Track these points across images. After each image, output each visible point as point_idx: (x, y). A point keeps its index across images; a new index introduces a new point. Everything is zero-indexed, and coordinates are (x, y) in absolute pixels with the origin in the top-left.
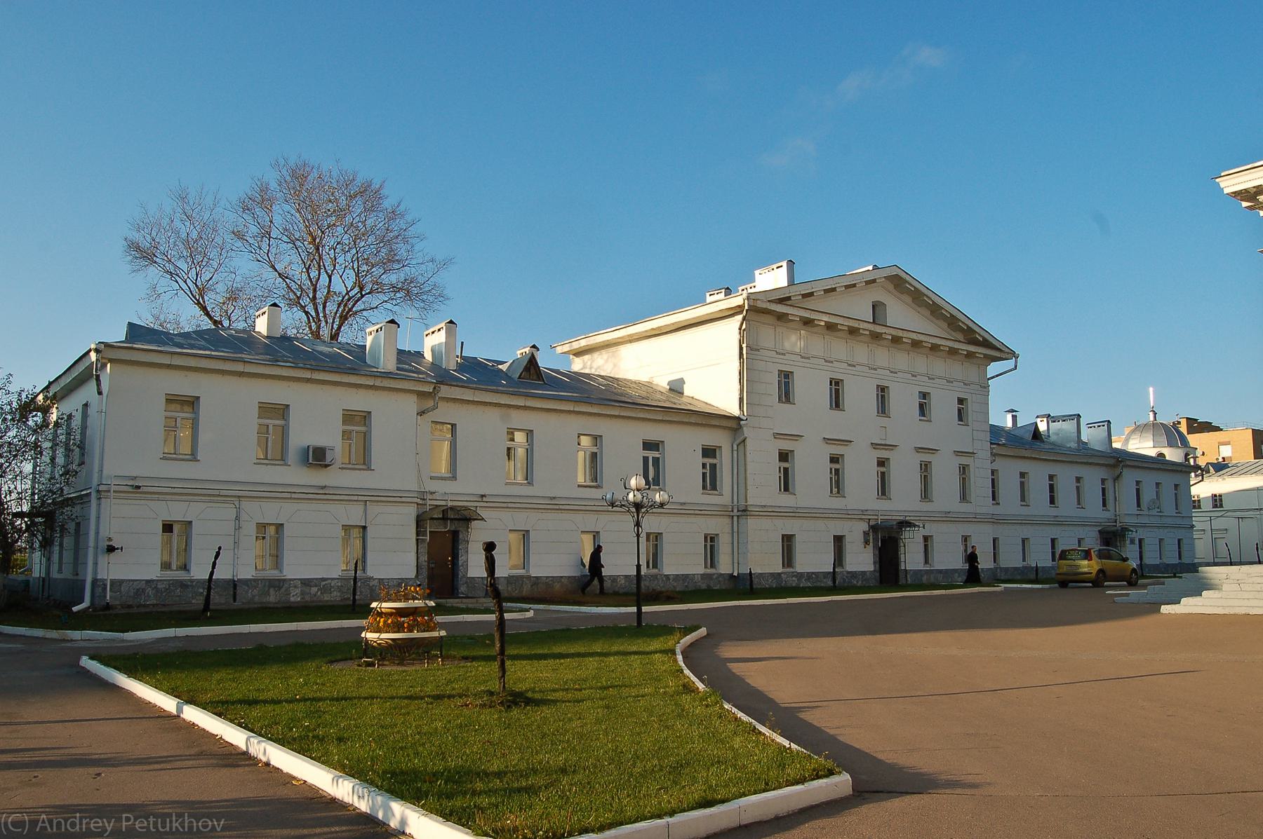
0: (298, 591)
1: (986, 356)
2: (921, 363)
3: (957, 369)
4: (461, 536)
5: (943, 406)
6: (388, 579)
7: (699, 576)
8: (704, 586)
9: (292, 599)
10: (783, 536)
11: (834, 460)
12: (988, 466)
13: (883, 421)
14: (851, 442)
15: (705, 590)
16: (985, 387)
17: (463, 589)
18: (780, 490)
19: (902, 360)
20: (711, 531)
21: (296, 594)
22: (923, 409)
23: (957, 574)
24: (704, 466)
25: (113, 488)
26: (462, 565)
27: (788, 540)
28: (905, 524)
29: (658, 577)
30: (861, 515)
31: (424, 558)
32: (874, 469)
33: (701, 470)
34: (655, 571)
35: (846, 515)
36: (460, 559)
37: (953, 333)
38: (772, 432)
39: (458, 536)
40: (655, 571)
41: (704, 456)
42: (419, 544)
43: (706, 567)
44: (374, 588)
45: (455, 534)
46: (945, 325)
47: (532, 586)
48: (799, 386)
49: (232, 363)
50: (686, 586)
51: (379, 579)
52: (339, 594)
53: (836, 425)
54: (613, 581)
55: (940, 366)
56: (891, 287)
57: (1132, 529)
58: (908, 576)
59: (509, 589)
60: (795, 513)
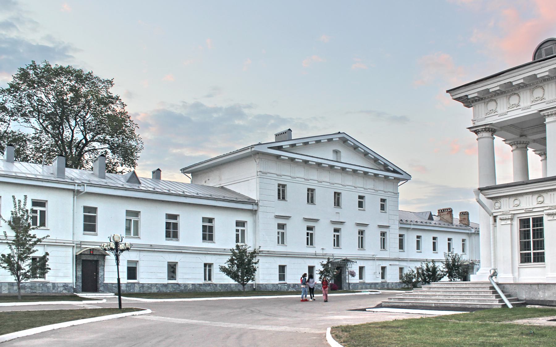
0: (7, 288)
1: (395, 178)
2: (360, 182)
3: (380, 186)
4: (100, 263)
5: (372, 203)
6: (58, 283)
7: (234, 285)
8: (237, 290)
9: (3, 292)
10: (280, 266)
11: (309, 228)
12: (398, 232)
13: (338, 210)
14: (368, 225)
15: (237, 292)
16: (396, 194)
17: (101, 289)
18: (278, 243)
19: (349, 181)
20: (362, 265)
21: (5, 290)
22: (361, 205)
23: (378, 285)
24: (278, 233)
25: (376, 258)
26: (101, 277)
27: (282, 268)
28: (346, 261)
29: (211, 285)
30: (323, 256)
31: (80, 273)
32: (379, 237)
33: (277, 235)
34: (209, 282)
35: (315, 256)
36: (100, 274)
37: (378, 166)
38: (273, 215)
39: (99, 263)
40: (209, 282)
41: (237, 225)
42: (77, 266)
43: (205, 279)
44: (49, 287)
45: (97, 261)
46: (373, 162)
47: (140, 288)
48: (367, 202)
49: (113, 190)
50: (227, 290)
51: (53, 283)
52: (29, 290)
53: (311, 212)
54: (185, 287)
55: (370, 184)
56: (342, 143)
57: (353, 261)
58: (350, 286)
59: (127, 289)
60: (179, 251)
